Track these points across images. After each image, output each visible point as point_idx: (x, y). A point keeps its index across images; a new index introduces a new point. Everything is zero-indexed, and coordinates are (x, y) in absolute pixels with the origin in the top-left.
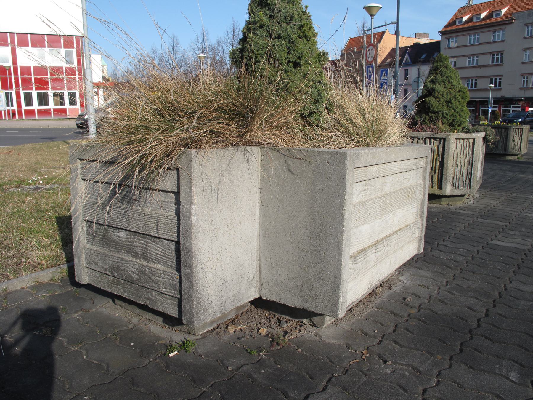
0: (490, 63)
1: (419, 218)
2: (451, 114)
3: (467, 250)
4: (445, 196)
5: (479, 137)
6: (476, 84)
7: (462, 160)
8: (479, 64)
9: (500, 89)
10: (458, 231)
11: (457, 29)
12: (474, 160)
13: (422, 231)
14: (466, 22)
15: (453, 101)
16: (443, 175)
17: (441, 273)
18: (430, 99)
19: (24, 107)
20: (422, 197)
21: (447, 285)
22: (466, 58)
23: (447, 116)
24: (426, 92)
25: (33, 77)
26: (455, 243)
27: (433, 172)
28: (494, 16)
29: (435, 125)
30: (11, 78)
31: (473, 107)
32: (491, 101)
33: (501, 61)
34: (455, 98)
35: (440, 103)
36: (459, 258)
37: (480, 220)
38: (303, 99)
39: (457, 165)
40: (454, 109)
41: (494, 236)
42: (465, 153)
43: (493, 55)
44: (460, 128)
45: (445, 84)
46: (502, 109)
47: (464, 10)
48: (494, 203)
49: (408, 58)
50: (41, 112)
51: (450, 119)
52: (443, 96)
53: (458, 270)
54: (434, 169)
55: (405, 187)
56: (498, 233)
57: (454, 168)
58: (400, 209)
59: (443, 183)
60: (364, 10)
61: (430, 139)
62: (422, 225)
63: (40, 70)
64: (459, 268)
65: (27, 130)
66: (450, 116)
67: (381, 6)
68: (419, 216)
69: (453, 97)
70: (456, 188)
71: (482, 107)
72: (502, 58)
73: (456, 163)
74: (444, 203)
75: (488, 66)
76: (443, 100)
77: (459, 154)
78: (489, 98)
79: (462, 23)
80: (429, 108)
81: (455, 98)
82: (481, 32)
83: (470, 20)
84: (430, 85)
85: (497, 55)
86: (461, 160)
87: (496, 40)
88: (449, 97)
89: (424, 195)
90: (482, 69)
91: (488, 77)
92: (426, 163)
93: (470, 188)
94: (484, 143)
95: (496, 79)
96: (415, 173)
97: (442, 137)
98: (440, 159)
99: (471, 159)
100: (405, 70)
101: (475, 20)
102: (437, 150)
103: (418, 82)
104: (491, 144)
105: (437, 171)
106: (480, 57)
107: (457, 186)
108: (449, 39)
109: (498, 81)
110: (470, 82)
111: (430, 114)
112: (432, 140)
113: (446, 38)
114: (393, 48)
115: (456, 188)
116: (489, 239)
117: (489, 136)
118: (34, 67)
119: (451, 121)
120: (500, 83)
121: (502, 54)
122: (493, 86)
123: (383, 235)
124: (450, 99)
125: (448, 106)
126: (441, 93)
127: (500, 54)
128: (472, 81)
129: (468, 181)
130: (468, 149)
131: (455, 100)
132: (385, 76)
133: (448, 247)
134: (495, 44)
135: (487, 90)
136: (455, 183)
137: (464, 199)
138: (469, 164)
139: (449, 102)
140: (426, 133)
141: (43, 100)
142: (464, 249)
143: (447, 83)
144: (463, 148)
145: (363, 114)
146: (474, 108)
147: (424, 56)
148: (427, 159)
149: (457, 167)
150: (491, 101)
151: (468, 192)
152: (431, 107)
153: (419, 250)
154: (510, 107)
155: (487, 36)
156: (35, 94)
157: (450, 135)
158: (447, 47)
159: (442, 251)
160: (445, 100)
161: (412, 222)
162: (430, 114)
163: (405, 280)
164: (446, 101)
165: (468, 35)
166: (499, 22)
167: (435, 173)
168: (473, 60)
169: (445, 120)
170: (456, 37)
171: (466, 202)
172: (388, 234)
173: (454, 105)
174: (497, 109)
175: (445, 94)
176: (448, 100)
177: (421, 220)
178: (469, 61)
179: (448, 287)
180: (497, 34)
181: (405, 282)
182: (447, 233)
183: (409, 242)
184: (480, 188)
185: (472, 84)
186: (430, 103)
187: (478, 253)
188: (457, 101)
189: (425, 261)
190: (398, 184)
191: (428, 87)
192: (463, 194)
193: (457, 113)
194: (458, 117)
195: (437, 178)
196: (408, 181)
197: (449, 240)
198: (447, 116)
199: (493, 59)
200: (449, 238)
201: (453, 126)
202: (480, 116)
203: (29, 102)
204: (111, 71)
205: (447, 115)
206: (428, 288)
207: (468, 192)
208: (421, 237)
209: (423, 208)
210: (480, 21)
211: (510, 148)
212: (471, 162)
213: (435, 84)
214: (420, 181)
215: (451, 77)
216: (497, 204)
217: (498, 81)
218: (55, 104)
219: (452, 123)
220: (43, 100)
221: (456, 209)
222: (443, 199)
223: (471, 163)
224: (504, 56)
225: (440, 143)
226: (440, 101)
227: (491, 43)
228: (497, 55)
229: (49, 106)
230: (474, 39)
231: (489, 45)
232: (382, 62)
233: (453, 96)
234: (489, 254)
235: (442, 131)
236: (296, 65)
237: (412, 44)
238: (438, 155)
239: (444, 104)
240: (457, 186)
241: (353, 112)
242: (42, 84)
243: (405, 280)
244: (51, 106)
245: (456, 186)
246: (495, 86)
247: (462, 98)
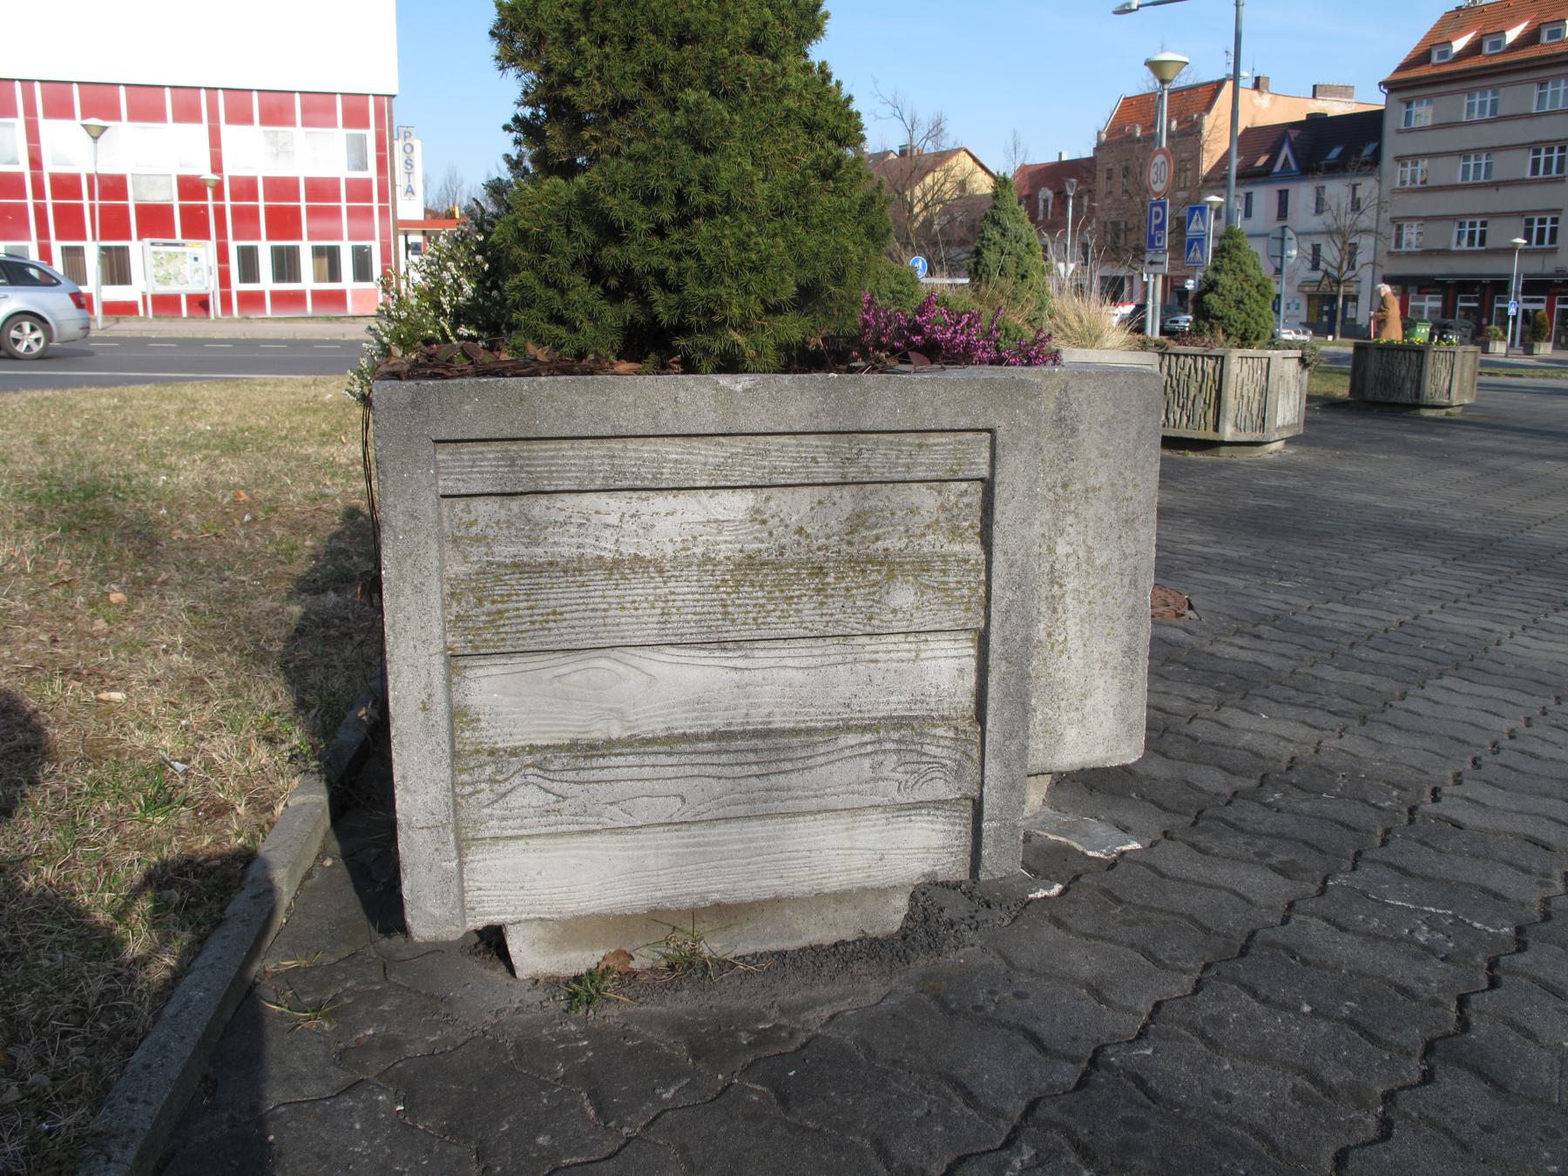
0: (1528, 175)
5: (1276, 356)
6: (1483, 234)
7: (1251, 390)
8: (1495, 177)
9: (1554, 251)
11: (1432, 77)
14: (1461, 56)
15: (1246, 301)
19: (237, 286)
22: (1456, 158)
25: (262, 204)
28: (1544, 39)
30: (91, 197)
31: (1476, 300)
32: (1516, 286)
38: (1030, 307)
43: (1537, 152)
46: (1558, 306)
47: (1455, 20)
50: (278, 298)
60: (1147, 68)
61: (1203, 356)
63: (282, 188)
65: (253, 344)
67: (1186, 60)
71: (1463, 300)
75: (1522, 182)
76: (1230, 299)
78: (1510, 275)
79: (1450, 58)
80: (1208, 311)
82: (1504, 85)
83: (1474, 49)
84: (1211, 275)
85: (1550, 151)
87: (1547, 109)
90: (1502, 190)
91: (1520, 214)
100: (1280, 192)
101: (1486, 50)
103: (1282, 240)
108: (1409, 104)
109: (1548, 226)
110: (1467, 229)
113: (1401, 100)
118: (265, 179)
120: (1554, 232)
127: (1556, 149)
128: (1472, 225)
129: (1260, 421)
134: (1544, 120)
135: (1510, 251)
141: (286, 265)
143: (1238, 271)
145: (1081, 321)
146: (1475, 305)
147: (1335, 153)
150: (1516, 286)
155: (1521, 96)
156: (264, 249)
158: (1402, 127)
165: (1463, 91)
166: (1558, 55)
168: (1477, 166)
170: (1429, 98)
173: (1248, 307)
174: (1542, 306)
178: (1466, 169)
185: (1472, 234)
194: (1253, 325)
199: (1536, 163)
202: (1493, 326)
203: (249, 271)
204: (438, 182)
210: (1503, 53)
218: (318, 279)
220: (286, 265)
222: (1223, 449)
227: (1530, 116)
228: (1550, 151)
229: (340, 280)
231: (1525, 122)
232: (1212, 170)
235: (1221, 346)
236: (1023, 277)
241: (1071, 318)
242: (284, 223)
244: (308, 282)
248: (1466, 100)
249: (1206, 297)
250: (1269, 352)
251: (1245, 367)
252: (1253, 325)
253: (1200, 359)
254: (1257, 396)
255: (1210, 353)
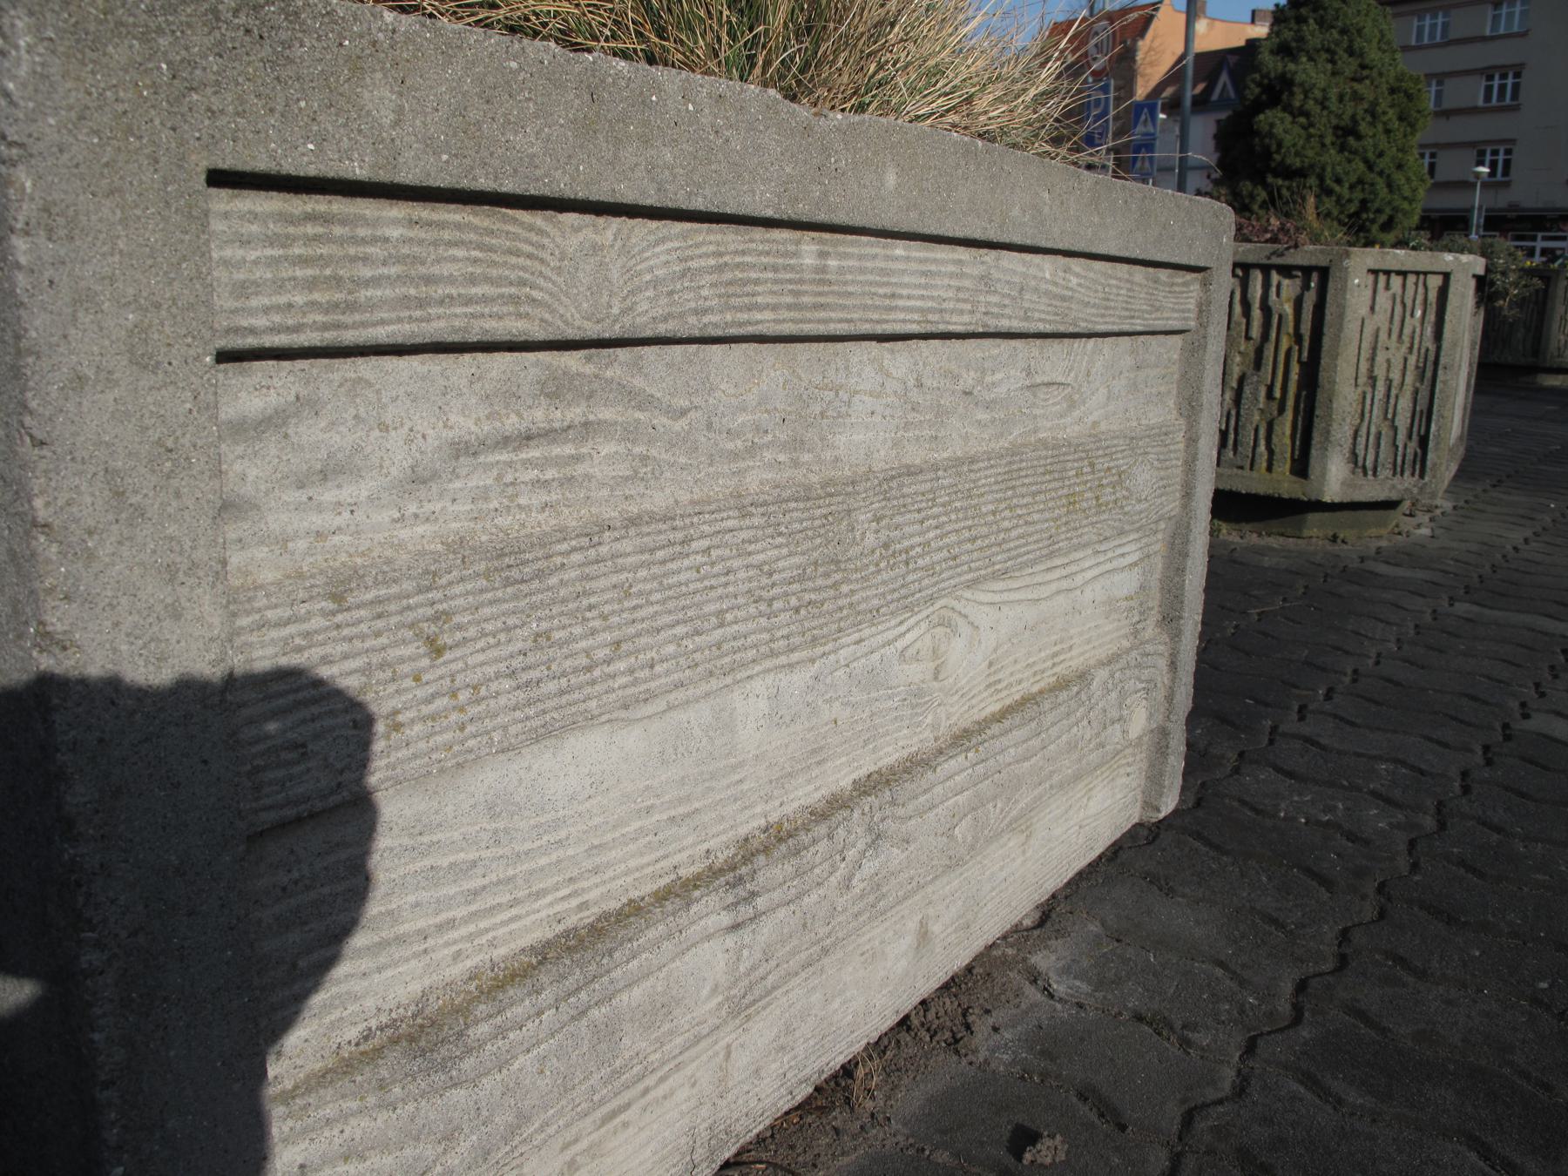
0: (1480, 103)
1: (1159, 624)
2: (1353, 179)
3: (1413, 768)
4: (1320, 506)
7: (1395, 360)
9: (1507, 184)
10: (1371, 662)
12: (1442, 361)
13: (1170, 698)
15: (1363, 127)
16: (1316, 420)
17: (1274, 921)
18: (1274, 121)
20: (1173, 506)
21: (1297, 1020)
23: (1337, 188)
24: (1257, 90)
26: (1352, 724)
27: (1275, 406)
29: (1287, 215)
32: (1476, 219)
33: (1515, 96)
34: (1373, 115)
35: (1310, 136)
36: (1376, 819)
37: (1461, 608)
39: (1373, 379)
40: (1366, 161)
41: (1533, 692)
42: (1407, 331)
43: (1490, 78)
44: (1391, 237)
45: (1333, 62)
48: (1517, 536)
49: (1229, 87)
51: (1350, 201)
52: (1324, 108)
53: (1364, 897)
54: (1277, 394)
55: (1044, 444)
56: (1547, 675)
57: (1360, 390)
58: (1000, 585)
59: (1314, 452)
61: (1266, 269)
62: (1173, 665)
64: (1370, 887)
66: (1352, 187)
68: (1154, 616)
69: (1366, 111)
70: (1365, 474)
72: (1516, 87)
73: (1371, 370)
74: (1315, 532)
75: (1474, 111)
76: (1323, 124)
77: (1383, 336)
78: (1470, 210)
80: (1267, 154)
81: (1373, 115)
85: (1504, 76)
86: (1388, 361)
87: (1502, 31)
88: (1349, 112)
89: (1188, 495)
91: (1472, 144)
92: (1203, 309)
93: (1422, 476)
94: (1478, 305)
95: (1495, 153)
96: (1129, 361)
97: (1314, 262)
98: (1305, 354)
99: (1431, 357)
102: (1291, 318)
104: (1510, 308)
105: (1290, 402)
106: (1450, 84)
107: (1369, 464)
111: (1270, 179)
112: (1275, 277)
114: (1215, 137)
115: (1365, 474)
116: (1514, 705)
117: (1504, 273)
119: (1352, 208)
120: (1507, 163)
121: (1517, 75)
122: (1485, 170)
123: (841, 777)
124: (1353, 117)
125: (1342, 149)
126: (1318, 94)
129: (1413, 445)
130: (1419, 313)
131: (1373, 124)
132: (1149, 123)
133: (1323, 748)
135: (1467, 185)
136: (1361, 453)
137: (1396, 517)
138: (1421, 377)
139: (1346, 132)
140: (1249, 246)
142: (1396, 761)
144: (1398, 309)
148: (1205, 284)
149: (1374, 387)
150: (1476, 219)
151: (1415, 491)
152: (1274, 147)
153: (1149, 805)
154: (1534, 239)
157: (1348, 255)
159: (1290, 775)
160: (1334, 121)
161: (1102, 654)
162: (1270, 179)
163: (1066, 971)
164: (1336, 128)
165: (1412, 13)
167: (1281, 410)
169: (1329, 204)
171: (1404, 528)
172: (890, 755)
175: (1334, 99)
176: (1346, 121)
177: (1165, 638)
179: (1305, 1033)
180: (1504, 10)
181: (1059, 988)
182: (1324, 669)
183: (1077, 777)
184: (1456, 477)
186: (1270, 135)
187: (1466, 790)
188: (1380, 127)
189: (1198, 836)
190: (982, 415)
191: (1265, 70)
192: (1394, 496)
193: (1381, 173)
194: (1383, 191)
195: (1288, 432)
196: (1072, 405)
197: (1328, 707)
198: (1337, 188)
199: (1489, 89)
200: (1328, 697)
201: (1362, 228)
205: (1338, 181)
206: (1185, 1043)
207: (1415, 491)
208: (1163, 732)
209: (1181, 571)
211: (1553, 345)
212: (1430, 370)
213: (1295, 59)
214: (1164, 413)
215: (1359, 31)
216: (1526, 541)
217: (1501, 158)
219: (1357, 214)
221: (1362, 559)
222: (1313, 517)
223: (1429, 374)
224: (1523, 80)
225: (1306, 287)
226: (1311, 125)
227: (1484, 39)
230: (1433, 26)
233: (1366, 106)
234: (1522, 795)
235: (1315, 239)
237: (1242, 43)
238: (1298, 338)
239: (1328, 141)
240: (1369, 464)
243: (1066, 971)
245: (1364, 467)
246: (1493, 174)
247: (1401, 119)
248: (1416, 23)
249: (1263, 119)
250: (1449, 257)
251: (1383, 299)
252: (1383, 191)
253: (1257, 278)
254: (1410, 378)
255: (1289, 260)
